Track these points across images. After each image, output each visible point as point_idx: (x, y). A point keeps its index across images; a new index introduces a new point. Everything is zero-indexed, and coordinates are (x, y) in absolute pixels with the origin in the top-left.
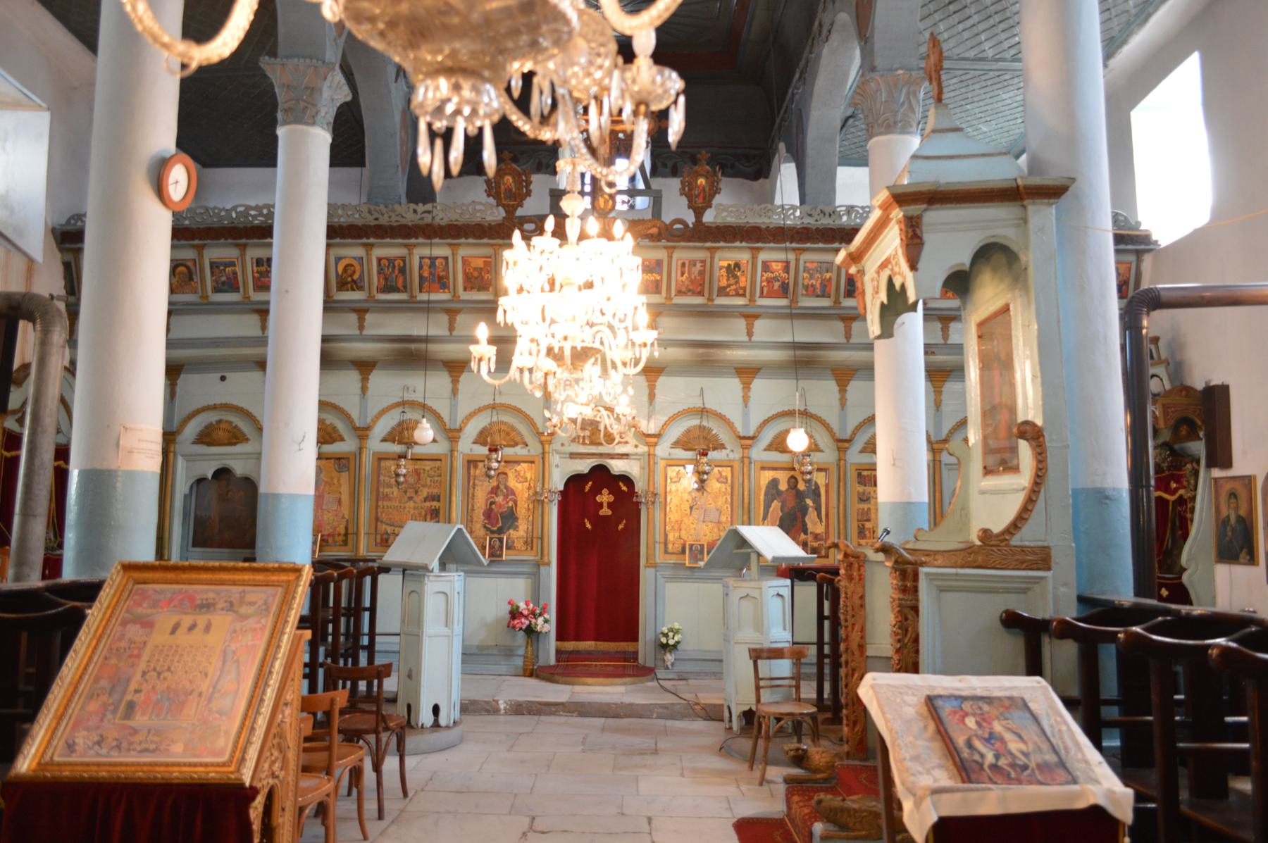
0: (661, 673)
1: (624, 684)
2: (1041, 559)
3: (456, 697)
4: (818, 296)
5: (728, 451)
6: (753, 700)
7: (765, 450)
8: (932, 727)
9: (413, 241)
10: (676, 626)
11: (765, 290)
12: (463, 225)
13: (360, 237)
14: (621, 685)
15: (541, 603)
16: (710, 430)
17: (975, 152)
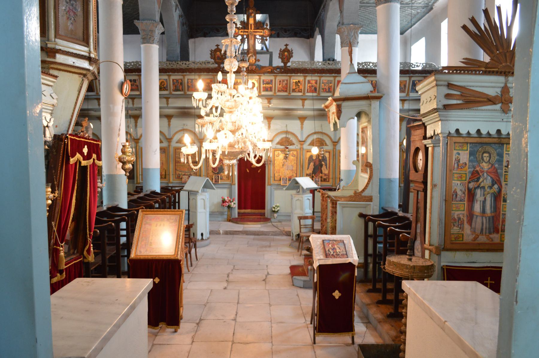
0: (272, 220)
1: (261, 224)
2: (370, 199)
3: (208, 231)
4: (327, 92)
5: (296, 146)
6: (299, 231)
7: (308, 145)
8: (322, 246)
9: (185, 74)
10: (278, 205)
11: (309, 90)
12: (203, 68)
13: (166, 72)
14: (259, 224)
15: (233, 198)
16: (289, 139)
17: (360, 81)
